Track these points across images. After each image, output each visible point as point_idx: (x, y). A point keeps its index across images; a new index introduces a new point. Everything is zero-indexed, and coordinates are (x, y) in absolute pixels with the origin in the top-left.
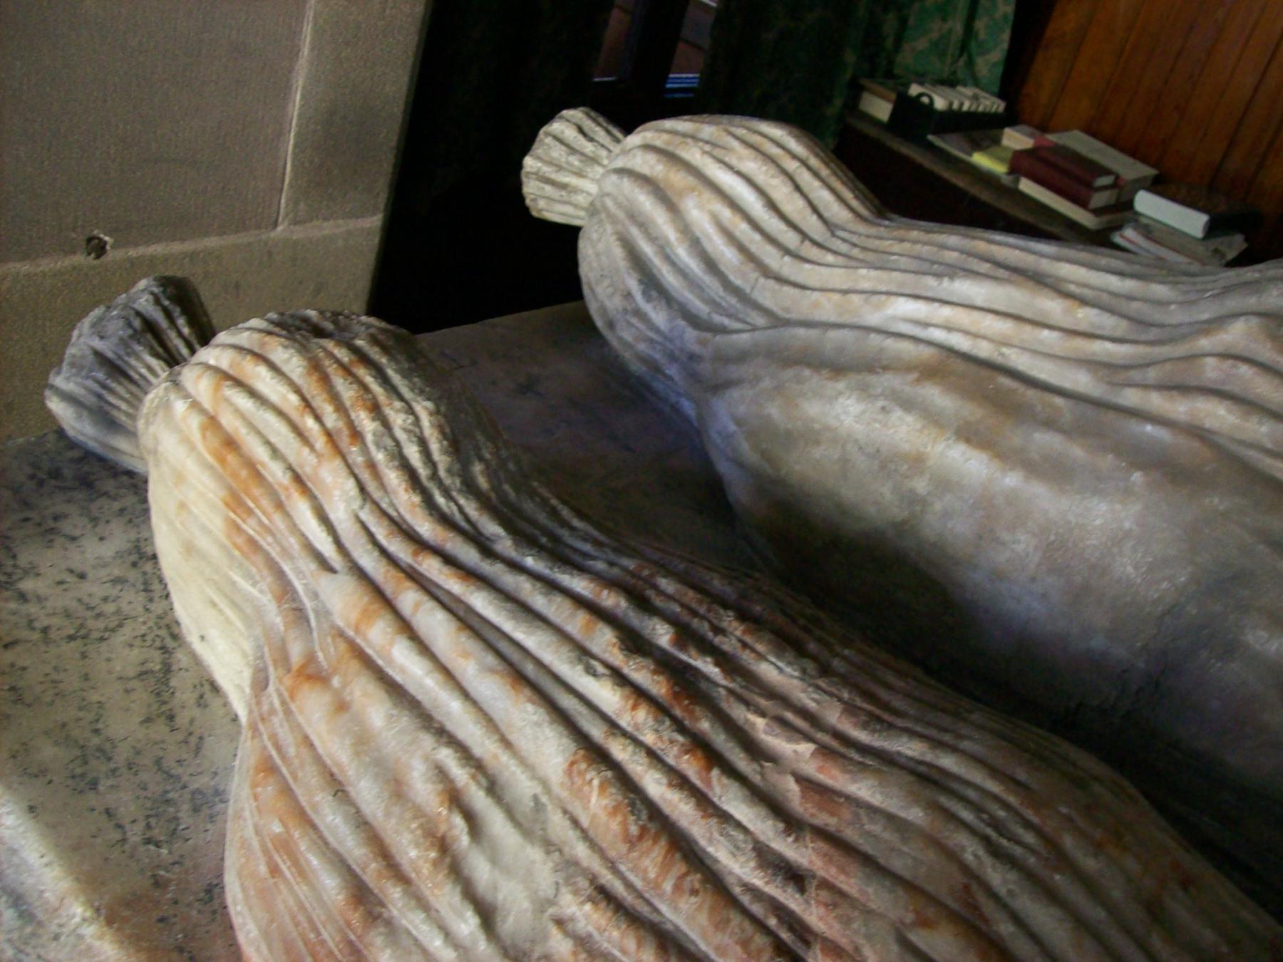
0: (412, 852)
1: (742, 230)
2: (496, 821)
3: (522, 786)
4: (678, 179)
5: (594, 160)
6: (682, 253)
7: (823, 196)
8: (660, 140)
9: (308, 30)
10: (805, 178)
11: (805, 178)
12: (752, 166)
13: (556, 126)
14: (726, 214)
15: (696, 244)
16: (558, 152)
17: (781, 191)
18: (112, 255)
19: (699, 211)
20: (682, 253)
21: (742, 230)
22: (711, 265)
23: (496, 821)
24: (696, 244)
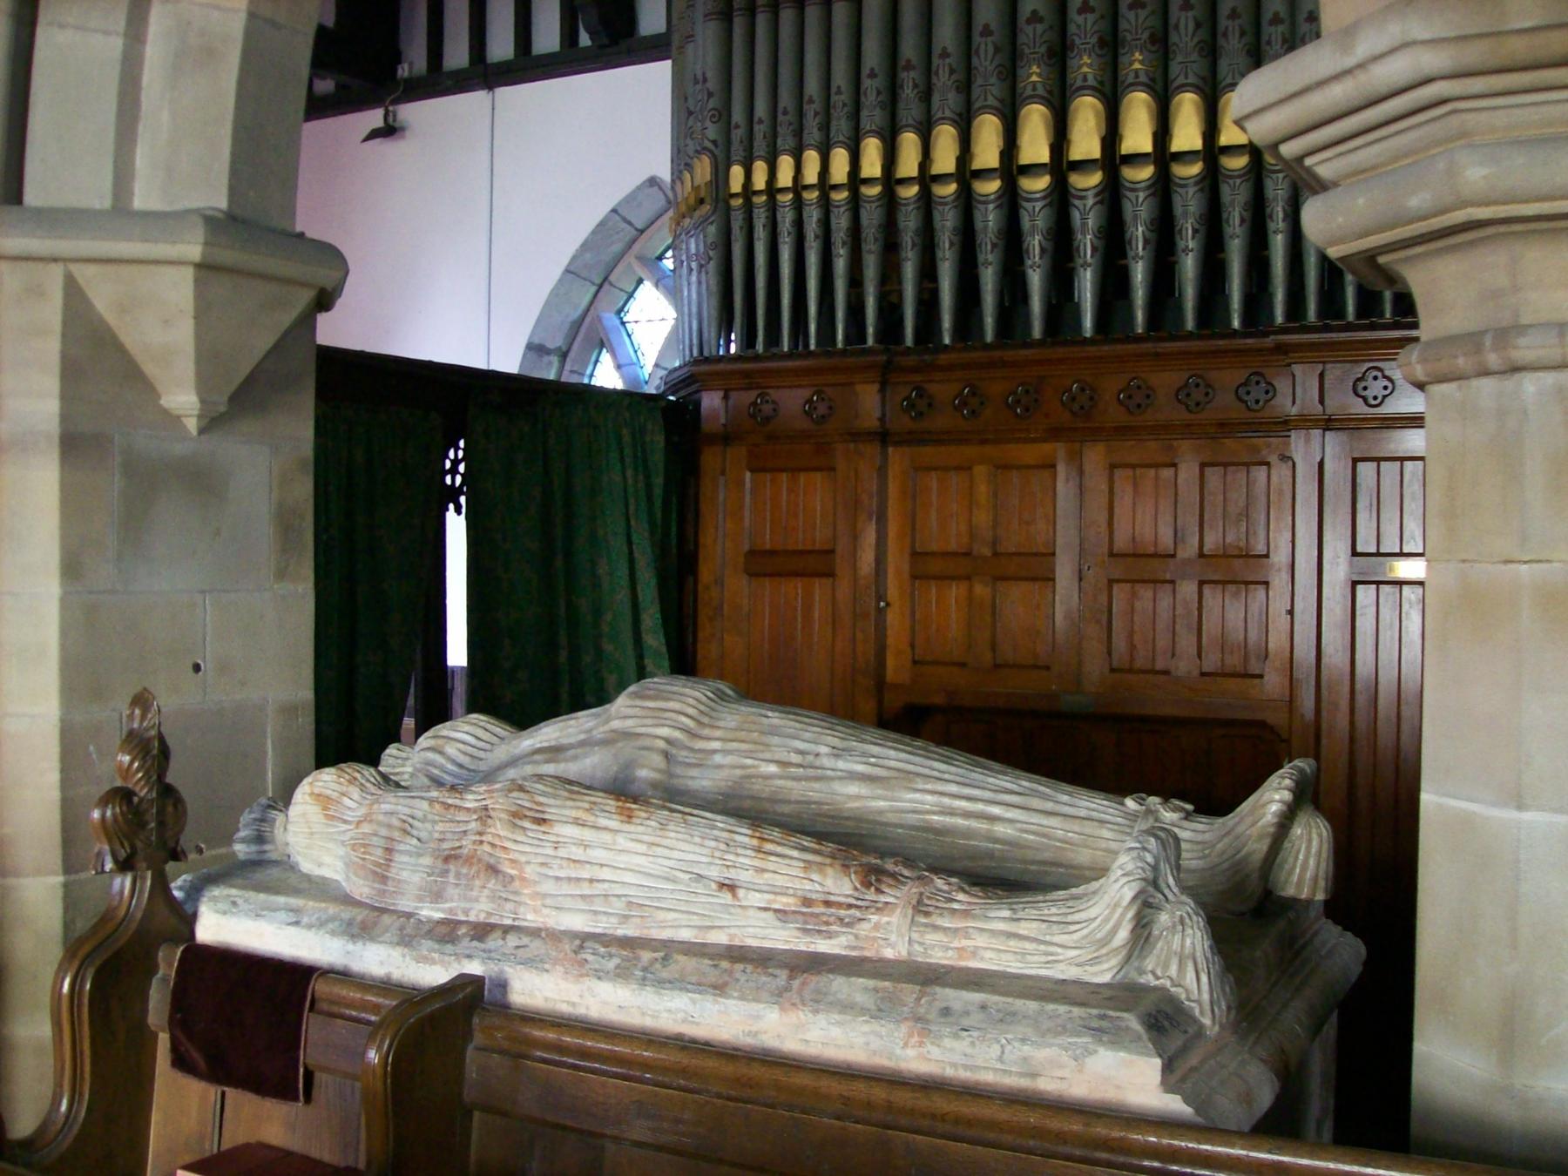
0: (396, 835)
1: (469, 749)
2: (416, 823)
3: (419, 814)
4: (440, 742)
5: (407, 759)
6: (450, 766)
7: (498, 730)
8: (431, 743)
9: (269, 742)
10: (489, 726)
11: (489, 726)
12: (467, 728)
13: (388, 751)
14: (461, 746)
15: (454, 762)
16: (391, 761)
17: (480, 733)
18: (207, 854)
19: (451, 750)
20: (450, 766)
21: (469, 749)
22: (461, 766)
23: (416, 823)
24: (454, 762)
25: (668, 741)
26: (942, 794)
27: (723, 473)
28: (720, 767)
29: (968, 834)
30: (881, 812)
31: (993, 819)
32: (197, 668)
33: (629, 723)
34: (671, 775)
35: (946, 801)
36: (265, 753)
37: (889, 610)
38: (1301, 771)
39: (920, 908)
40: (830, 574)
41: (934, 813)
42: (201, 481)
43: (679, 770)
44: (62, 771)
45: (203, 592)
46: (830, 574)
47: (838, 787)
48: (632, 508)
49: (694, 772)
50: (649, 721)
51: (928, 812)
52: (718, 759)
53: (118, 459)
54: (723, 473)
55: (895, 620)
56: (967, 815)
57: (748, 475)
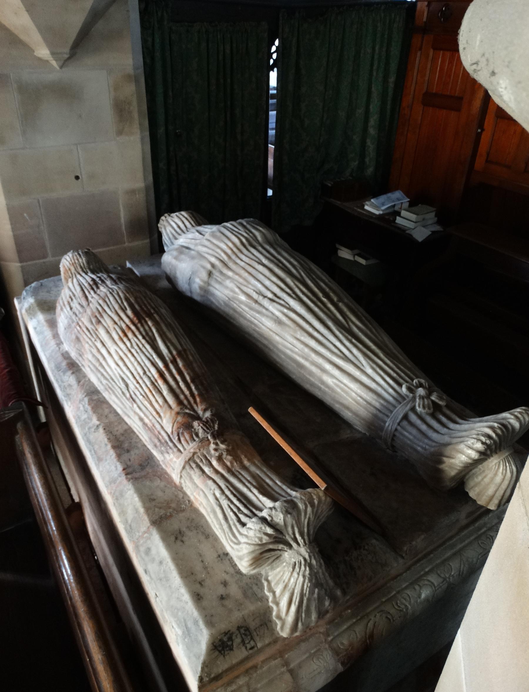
25: (213, 265)
26: (307, 345)
27: (420, 49)
28: (227, 287)
29: (311, 373)
30: (278, 343)
31: (324, 370)
32: (77, 178)
33: (205, 249)
34: (209, 284)
35: (306, 350)
36: (120, 211)
37: (484, 133)
38: (504, 426)
39: (191, 461)
40: (458, 110)
41: (299, 355)
42: (67, 93)
43: (213, 283)
44: (12, 224)
45: (76, 144)
46: (458, 110)
47: (264, 320)
48: (375, 67)
49: (217, 286)
50: (210, 252)
51: (296, 353)
52: (228, 283)
53: (15, 86)
54: (420, 49)
55: (486, 138)
56: (314, 363)
57: (432, 51)
